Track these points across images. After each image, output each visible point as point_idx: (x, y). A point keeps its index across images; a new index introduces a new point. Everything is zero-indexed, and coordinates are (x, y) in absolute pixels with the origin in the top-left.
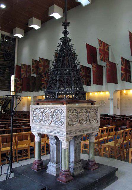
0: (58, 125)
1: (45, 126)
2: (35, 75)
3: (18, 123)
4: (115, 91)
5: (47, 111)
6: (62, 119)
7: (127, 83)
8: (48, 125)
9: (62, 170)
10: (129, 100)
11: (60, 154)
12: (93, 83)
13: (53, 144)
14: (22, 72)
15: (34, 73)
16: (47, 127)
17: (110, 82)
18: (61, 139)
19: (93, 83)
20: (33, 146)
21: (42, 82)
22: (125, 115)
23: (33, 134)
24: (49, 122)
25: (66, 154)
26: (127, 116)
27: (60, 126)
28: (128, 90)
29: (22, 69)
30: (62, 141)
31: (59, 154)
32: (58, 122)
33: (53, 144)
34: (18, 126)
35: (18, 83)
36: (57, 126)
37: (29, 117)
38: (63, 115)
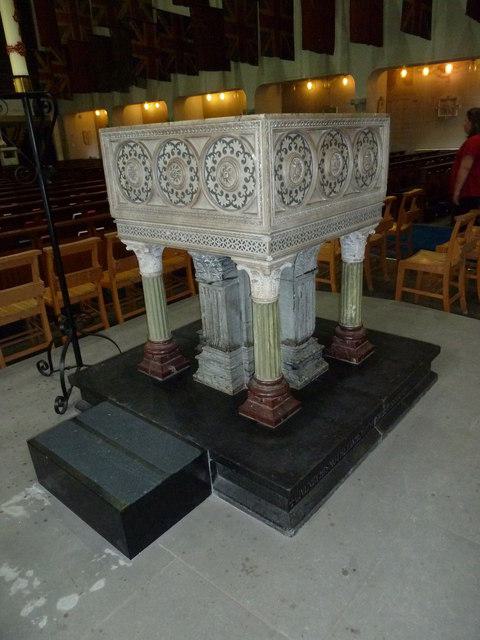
0: (231, 207)
1: (173, 214)
2: (106, 32)
3: (73, 200)
4: (373, 73)
5: (176, 151)
6: (247, 181)
7: (414, 41)
8: (187, 209)
9: (260, 382)
10: (416, 101)
11: (241, 318)
12: (305, 47)
13: (210, 284)
14: (59, 24)
15: (102, 24)
16: (180, 219)
17: (356, 42)
18: (248, 270)
19: (305, 47)
20: (98, 157)
21: (135, 56)
22: (402, 153)
23: (128, 249)
24: (187, 199)
25: (271, 323)
26: (411, 156)
27: (238, 213)
28: (415, 68)
29: (56, 10)
30: (250, 274)
31: (238, 318)
32: (231, 195)
33: (210, 284)
34: (73, 200)
35: (54, 62)
36: (226, 213)
37: (141, 287)
38: (249, 164)
